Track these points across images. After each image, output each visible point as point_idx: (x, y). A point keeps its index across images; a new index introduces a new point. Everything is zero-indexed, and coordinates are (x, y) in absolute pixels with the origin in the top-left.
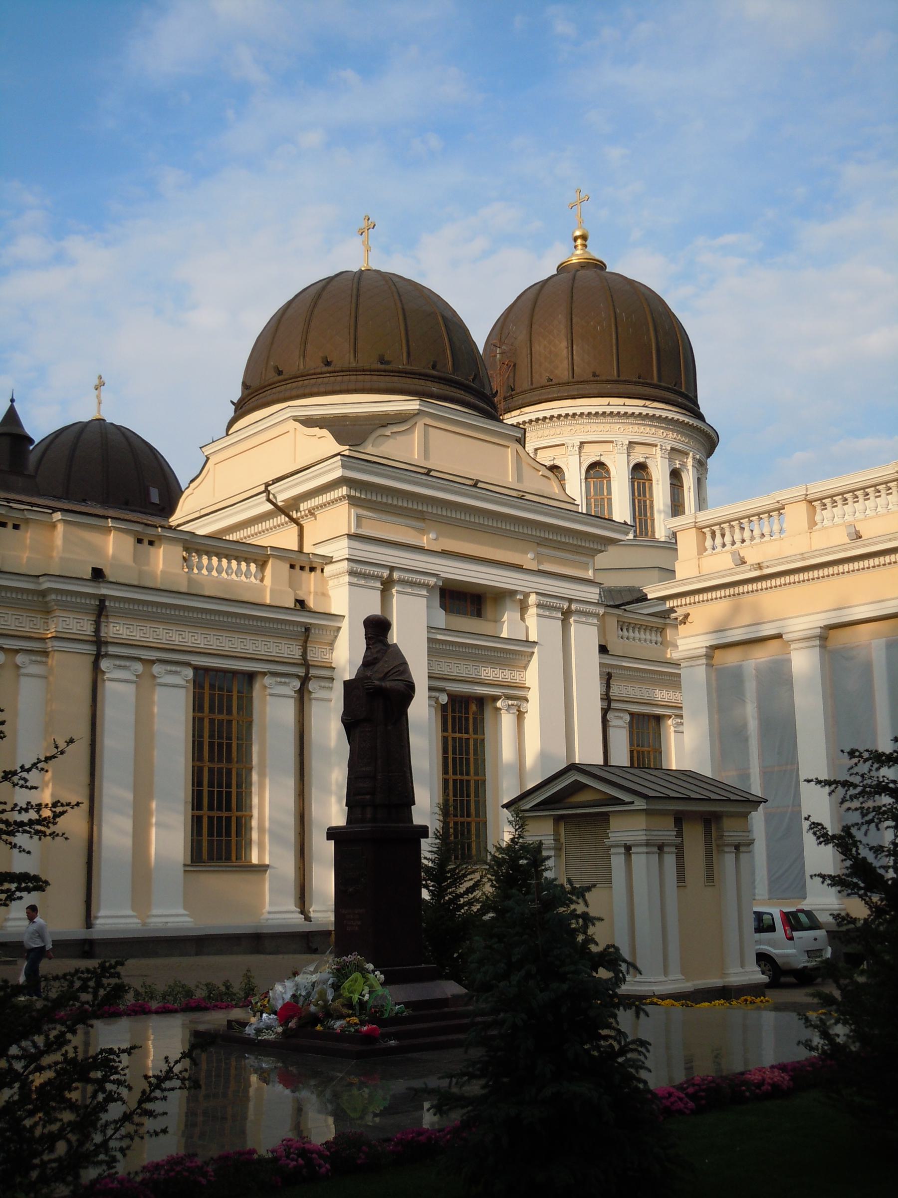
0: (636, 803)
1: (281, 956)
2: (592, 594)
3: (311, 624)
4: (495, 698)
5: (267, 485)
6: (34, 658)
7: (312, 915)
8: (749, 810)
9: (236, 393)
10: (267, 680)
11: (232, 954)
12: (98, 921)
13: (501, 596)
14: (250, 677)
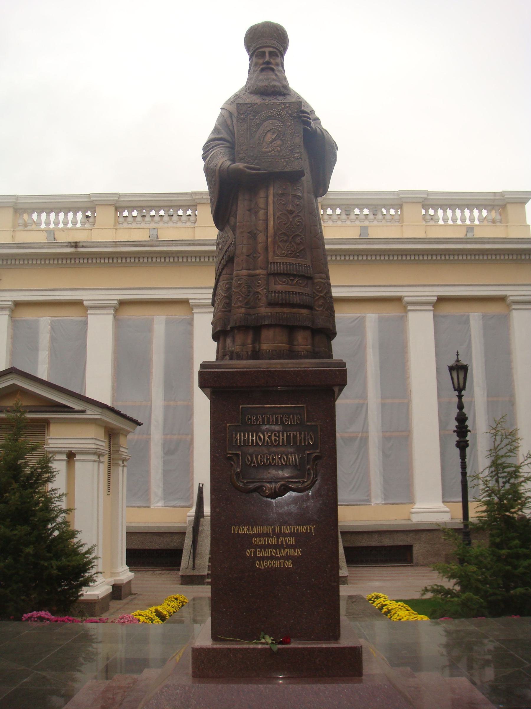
0: (88, 412)
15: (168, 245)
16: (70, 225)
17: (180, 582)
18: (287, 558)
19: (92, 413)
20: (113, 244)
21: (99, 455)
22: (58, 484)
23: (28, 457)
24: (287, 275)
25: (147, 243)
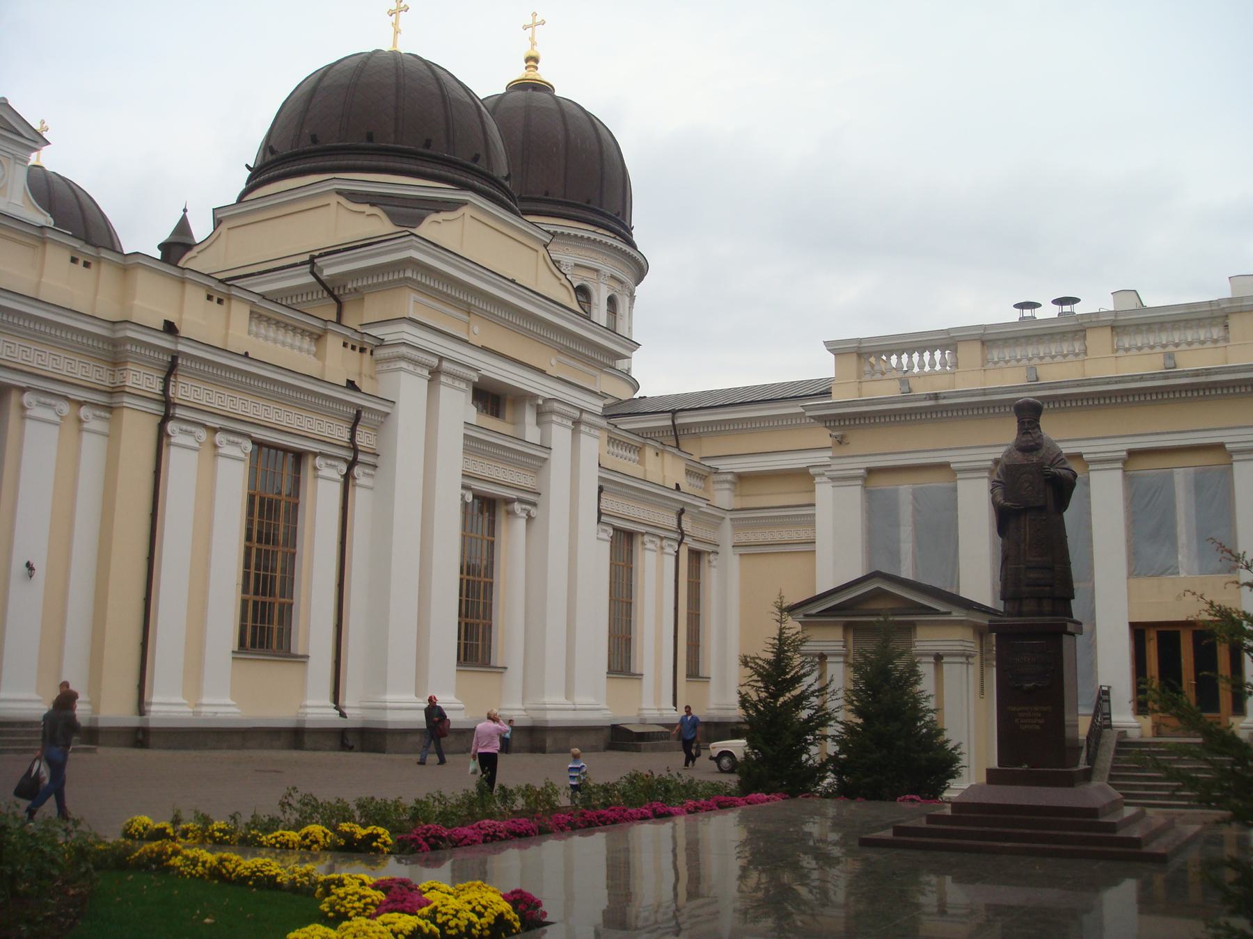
0: (954, 614)
2: (597, 406)
3: (363, 407)
4: (508, 501)
6: (98, 413)
7: (346, 711)
10: (319, 461)
12: (153, 708)
13: (520, 398)
14: (299, 457)
15: (1051, 388)
16: (927, 369)
19: (958, 614)
21: (968, 657)
22: (926, 685)
23: (897, 662)
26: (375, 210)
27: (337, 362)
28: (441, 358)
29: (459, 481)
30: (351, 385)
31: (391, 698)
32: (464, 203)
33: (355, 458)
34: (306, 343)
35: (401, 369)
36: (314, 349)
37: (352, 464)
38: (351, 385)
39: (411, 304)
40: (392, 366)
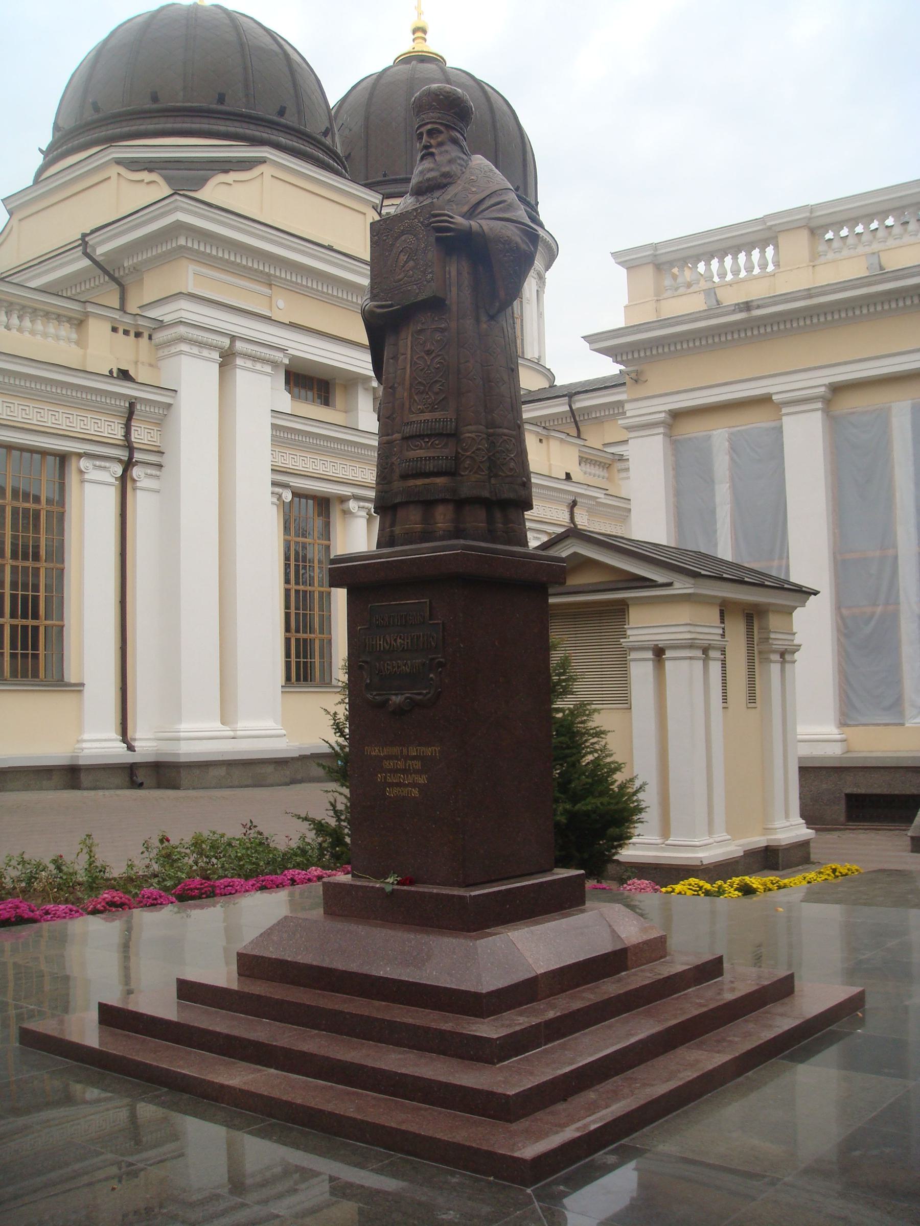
0: (677, 585)
1: (100, 793)
3: (136, 398)
4: (343, 499)
5: (84, 236)
6: (149, 471)
7: (136, 744)
8: (796, 604)
9: (46, 138)
10: (84, 463)
11: (41, 789)
14: (63, 458)
17: (909, 848)
18: (414, 785)
20: (805, 293)
24: (420, 436)
25: (858, 282)
26: (154, 176)
27: (103, 349)
28: (233, 338)
29: (268, 477)
30: (124, 375)
31: (187, 727)
32: (262, 161)
33: (131, 457)
34: (65, 330)
35: (181, 353)
36: (74, 336)
37: (128, 465)
38: (124, 375)
39: (189, 276)
40: (173, 350)
